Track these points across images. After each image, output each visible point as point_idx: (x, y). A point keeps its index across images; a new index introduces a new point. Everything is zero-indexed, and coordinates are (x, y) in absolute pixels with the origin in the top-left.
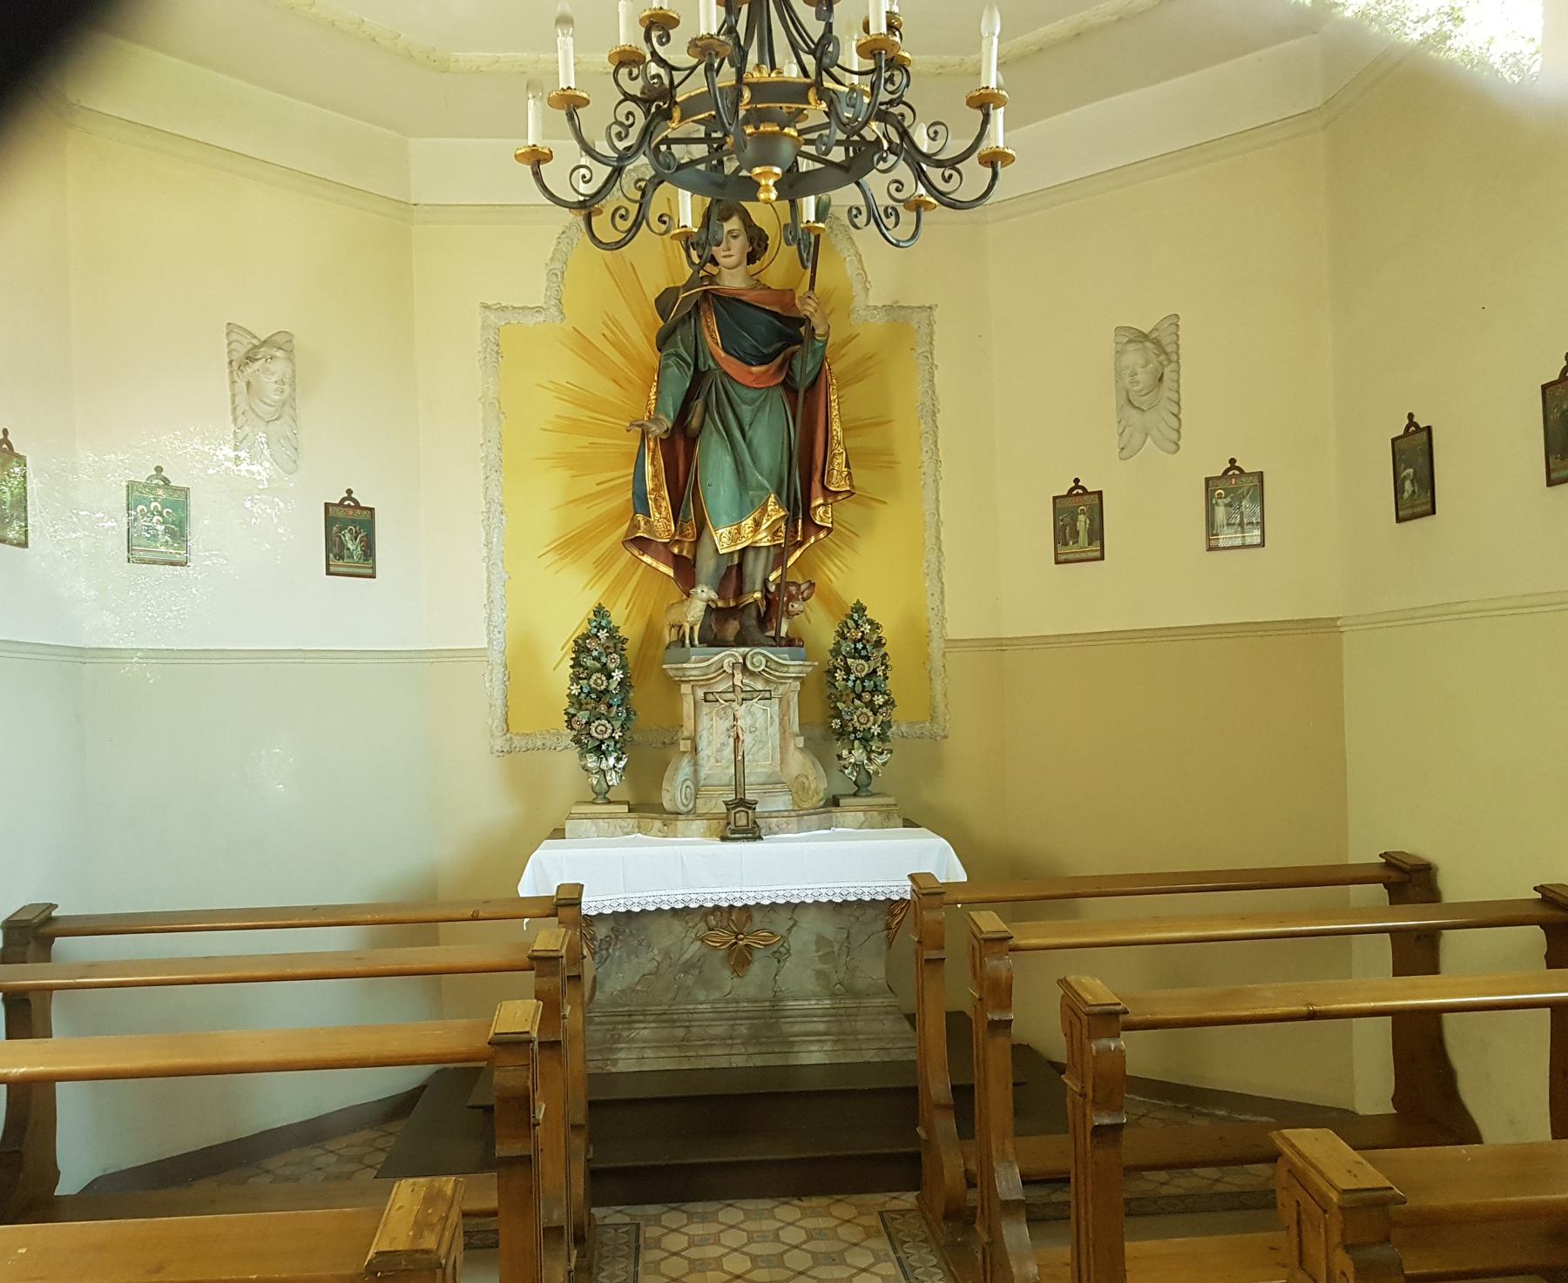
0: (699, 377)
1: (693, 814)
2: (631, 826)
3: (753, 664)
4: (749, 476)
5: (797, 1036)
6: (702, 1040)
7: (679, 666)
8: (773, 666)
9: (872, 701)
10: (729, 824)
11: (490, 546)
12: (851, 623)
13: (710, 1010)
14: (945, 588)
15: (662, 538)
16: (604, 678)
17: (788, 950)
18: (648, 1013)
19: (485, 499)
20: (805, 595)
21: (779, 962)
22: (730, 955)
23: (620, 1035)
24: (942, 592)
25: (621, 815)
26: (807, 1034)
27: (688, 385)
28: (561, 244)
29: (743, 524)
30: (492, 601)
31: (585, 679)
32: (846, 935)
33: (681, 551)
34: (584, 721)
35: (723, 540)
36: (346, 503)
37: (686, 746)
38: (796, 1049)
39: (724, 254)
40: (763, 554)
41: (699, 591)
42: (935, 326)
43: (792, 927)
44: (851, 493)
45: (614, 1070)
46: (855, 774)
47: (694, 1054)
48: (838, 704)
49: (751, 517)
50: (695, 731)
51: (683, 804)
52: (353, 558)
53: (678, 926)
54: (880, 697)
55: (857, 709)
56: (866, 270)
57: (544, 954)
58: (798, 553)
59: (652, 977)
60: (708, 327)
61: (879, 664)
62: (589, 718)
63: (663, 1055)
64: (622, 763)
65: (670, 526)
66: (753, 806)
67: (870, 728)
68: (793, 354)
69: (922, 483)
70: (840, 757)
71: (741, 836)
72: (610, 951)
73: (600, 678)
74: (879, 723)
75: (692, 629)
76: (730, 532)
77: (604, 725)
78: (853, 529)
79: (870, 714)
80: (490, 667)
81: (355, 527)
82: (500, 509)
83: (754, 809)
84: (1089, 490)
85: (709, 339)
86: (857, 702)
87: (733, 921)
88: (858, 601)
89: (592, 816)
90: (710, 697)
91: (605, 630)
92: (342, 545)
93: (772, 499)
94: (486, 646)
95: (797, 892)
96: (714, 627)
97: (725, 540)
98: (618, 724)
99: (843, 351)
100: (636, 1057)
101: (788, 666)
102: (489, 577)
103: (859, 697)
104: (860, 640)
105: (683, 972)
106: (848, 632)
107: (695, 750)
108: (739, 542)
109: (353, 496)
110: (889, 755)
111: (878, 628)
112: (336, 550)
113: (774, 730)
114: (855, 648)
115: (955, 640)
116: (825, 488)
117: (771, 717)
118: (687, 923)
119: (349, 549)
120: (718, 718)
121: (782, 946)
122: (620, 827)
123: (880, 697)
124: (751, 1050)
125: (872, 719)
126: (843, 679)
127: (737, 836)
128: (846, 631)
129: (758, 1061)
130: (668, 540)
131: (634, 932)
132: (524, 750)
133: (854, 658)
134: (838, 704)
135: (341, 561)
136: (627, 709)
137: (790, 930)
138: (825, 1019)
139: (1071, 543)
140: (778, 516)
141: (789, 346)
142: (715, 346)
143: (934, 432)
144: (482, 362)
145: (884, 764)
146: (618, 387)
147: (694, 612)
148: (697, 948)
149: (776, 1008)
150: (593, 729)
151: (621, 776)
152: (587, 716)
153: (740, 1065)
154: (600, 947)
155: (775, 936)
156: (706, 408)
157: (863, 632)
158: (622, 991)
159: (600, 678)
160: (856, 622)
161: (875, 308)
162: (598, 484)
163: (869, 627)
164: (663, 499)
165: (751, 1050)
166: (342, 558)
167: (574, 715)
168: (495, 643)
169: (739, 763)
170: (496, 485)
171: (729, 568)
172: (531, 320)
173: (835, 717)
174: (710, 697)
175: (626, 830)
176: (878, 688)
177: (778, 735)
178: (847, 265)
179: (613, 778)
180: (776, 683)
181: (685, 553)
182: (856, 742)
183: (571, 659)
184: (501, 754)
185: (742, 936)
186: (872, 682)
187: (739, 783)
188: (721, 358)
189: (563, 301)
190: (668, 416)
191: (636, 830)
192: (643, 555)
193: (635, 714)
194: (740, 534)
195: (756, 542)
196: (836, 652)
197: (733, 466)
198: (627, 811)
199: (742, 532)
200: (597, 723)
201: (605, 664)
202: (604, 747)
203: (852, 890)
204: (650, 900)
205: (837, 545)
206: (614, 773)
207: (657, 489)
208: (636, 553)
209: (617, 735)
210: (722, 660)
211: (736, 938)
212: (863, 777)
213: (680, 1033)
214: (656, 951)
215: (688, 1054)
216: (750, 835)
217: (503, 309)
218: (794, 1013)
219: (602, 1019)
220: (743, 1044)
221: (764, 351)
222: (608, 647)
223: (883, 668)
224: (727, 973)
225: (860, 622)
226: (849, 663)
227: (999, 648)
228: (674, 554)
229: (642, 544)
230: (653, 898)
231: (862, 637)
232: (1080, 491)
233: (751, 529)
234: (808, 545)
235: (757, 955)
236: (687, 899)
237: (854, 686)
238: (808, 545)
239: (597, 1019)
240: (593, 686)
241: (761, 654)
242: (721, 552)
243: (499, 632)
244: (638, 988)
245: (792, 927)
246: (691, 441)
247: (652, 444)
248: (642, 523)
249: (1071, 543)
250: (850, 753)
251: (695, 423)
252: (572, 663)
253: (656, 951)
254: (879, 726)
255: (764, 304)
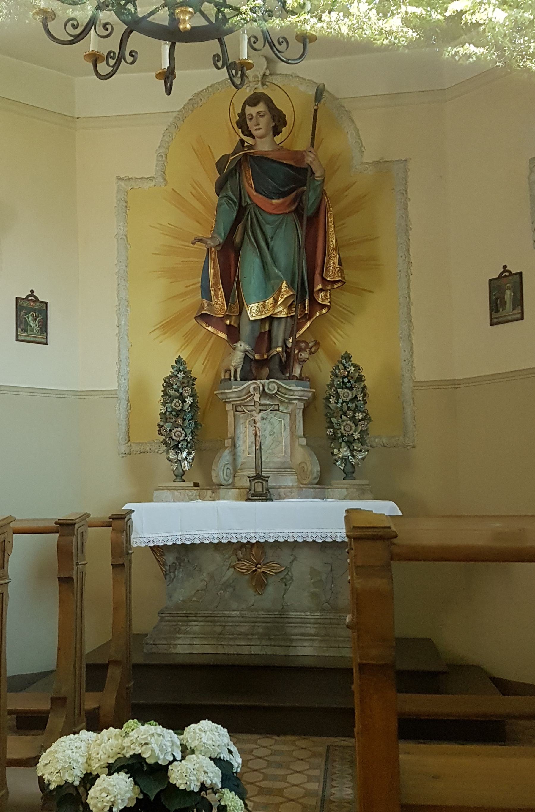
0: (242, 211)
1: (232, 486)
2: (194, 495)
3: (269, 389)
4: (269, 268)
5: (296, 635)
6: (233, 634)
7: (223, 391)
8: (283, 391)
9: (354, 417)
10: (250, 490)
11: (120, 327)
12: (341, 366)
13: (239, 615)
14: (414, 347)
15: (219, 315)
16: (180, 402)
17: (292, 578)
18: (199, 615)
19: (117, 297)
20: (313, 350)
21: (286, 585)
22: (252, 578)
23: (180, 629)
24: (412, 349)
25: (188, 488)
26: (302, 635)
27: (235, 216)
28: (165, 137)
29: (267, 302)
30: (121, 361)
31: (169, 403)
32: (330, 568)
33: (230, 322)
34: (168, 429)
35: (253, 311)
36: (30, 298)
37: (228, 443)
38: (294, 644)
39: (255, 128)
40: (283, 321)
41: (239, 345)
42: (409, 173)
43: (293, 561)
44: (342, 282)
45: (174, 652)
46: (343, 465)
47: (226, 643)
48: (332, 419)
49: (272, 298)
50: (234, 433)
51: (225, 479)
52: (33, 331)
53: (218, 557)
54: (360, 414)
55: (343, 421)
56: (362, 139)
57: (64, 522)
58: (308, 324)
59: (203, 592)
60: (246, 177)
61: (359, 393)
62: (171, 427)
63: (206, 643)
64: (192, 456)
65: (224, 307)
66: (267, 479)
67: (352, 434)
68: (303, 192)
69: (399, 277)
70: (332, 454)
71: (258, 498)
72: (176, 573)
73: (178, 402)
74: (359, 431)
75: (236, 371)
76: (257, 307)
77: (180, 432)
78: (349, 309)
79: (352, 425)
80: (119, 401)
81: (35, 313)
82: (126, 303)
83: (267, 481)
84: (513, 272)
85: (246, 184)
86: (344, 417)
87: (253, 554)
88: (346, 352)
89: (171, 488)
90: (239, 409)
91: (182, 373)
92: (27, 324)
93: (284, 284)
94: (117, 388)
95: (292, 534)
96: (254, 372)
97: (254, 311)
98: (189, 431)
99: (346, 194)
100: (188, 643)
101: (293, 390)
102: (119, 346)
103: (345, 414)
104: (346, 377)
105: (223, 590)
106: (339, 372)
107: (234, 445)
108: (264, 313)
109: (34, 294)
110: (366, 453)
111: (360, 369)
112: (23, 326)
113: (286, 434)
114: (343, 382)
115: (422, 382)
116: (324, 279)
117: (284, 425)
118: (224, 556)
119: (31, 326)
120: (250, 426)
121: (287, 574)
122: (188, 496)
123: (360, 414)
124: (264, 643)
125: (353, 428)
126: (335, 403)
127: (256, 498)
128: (337, 371)
129: (269, 651)
130: (222, 316)
131: (190, 561)
132: (138, 453)
133: (342, 388)
134: (332, 419)
135: (26, 333)
136: (195, 422)
137: (291, 563)
138: (316, 626)
139: (501, 309)
140: (288, 295)
141: (301, 187)
142: (250, 189)
143: (407, 243)
144: (117, 213)
145: (363, 459)
146: (199, 225)
147: (237, 358)
148: (232, 572)
149: (283, 616)
150: (173, 434)
151: (191, 465)
152: (171, 426)
153: (256, 653)
154: (169, 569)
155: (282, 567)
156: (245, 230)
157: (349, 372)
158: (184, 601)
159: (178, 402)
160: (344, 365)
161: (368, 163)
162: (187, 287)
163: (353, 369)
164: (219, 289)
165: (264, 643)
166: (26, 331)
167: (163, 426)
168: (122, 386)
169: (258, 452)
170: (124, 289)
171: (262, 334)
172: (146, 186)
173: (329, 428)
174: (239, 409)
175: (192, 497)
176: (359, 408)
177: (289, 437)
178: (349, 136)
179: (186, 466)
180: (287, 403)
181: (232, 323)
182: (343, 444)
183: (162, 391)
184: (124, 455)
185: (260, 566)
186: (354, 405)
187: (258, 466)
188: (253, 195)
189: (166, 173)
190: (220, 235)
191: (198, 498)
192: (208, 327)
193: (201, 426)
194: (265, 308)
195: (276, 314)
196: (331, 385)
197: (261, 264)
198: (192, 485)
199: (266, 307)
200: (175, 430)
201: (182, 393)
202: (180, 446)
203: (329, 535)
204: (197, 536)
205: (339, 321)
206: (186, 462)
207: (216, 284)
208: (204, 325)
209: (189, 438)
210: (249, 386)
211: (256, 567)
212: (349, 466)
213: (218, 629)
214: (205, 574)
215: (223, 643)
216: (264, 498)
217: (129, 179)
218: (294, 620)
219: (169, 618)
220: (259, 639)
221: (281, 189)
222: (184, 383)
223: (362, 395)
224: (251, 592)
225: (347, 365)
226: (339, 392)
227: (453, 386)
228: (227, 325)
229: (204, 317)
230: (198, 536)
231: (348, 375)
232: (507, 274)
233: (272, 305)
234: (315, 317)
235: (271, 580)
236: (220, 536)
237: (342, 407)
238: (315, 317)
239: (167, 618)
240: (174, 407)
241: (275, 382)
242: (252, 319)
243: (125, 379)
244: (194, 599)
245: (293, 561)
246: (238, 251)
247: (213, 255)
248: (206, 305)
249: (501, 309)
250: (339, 451)
251: (238, 239)
252: (162, 394)
253: (205, 574)
254: (359, 433)
255: (282, 159)
